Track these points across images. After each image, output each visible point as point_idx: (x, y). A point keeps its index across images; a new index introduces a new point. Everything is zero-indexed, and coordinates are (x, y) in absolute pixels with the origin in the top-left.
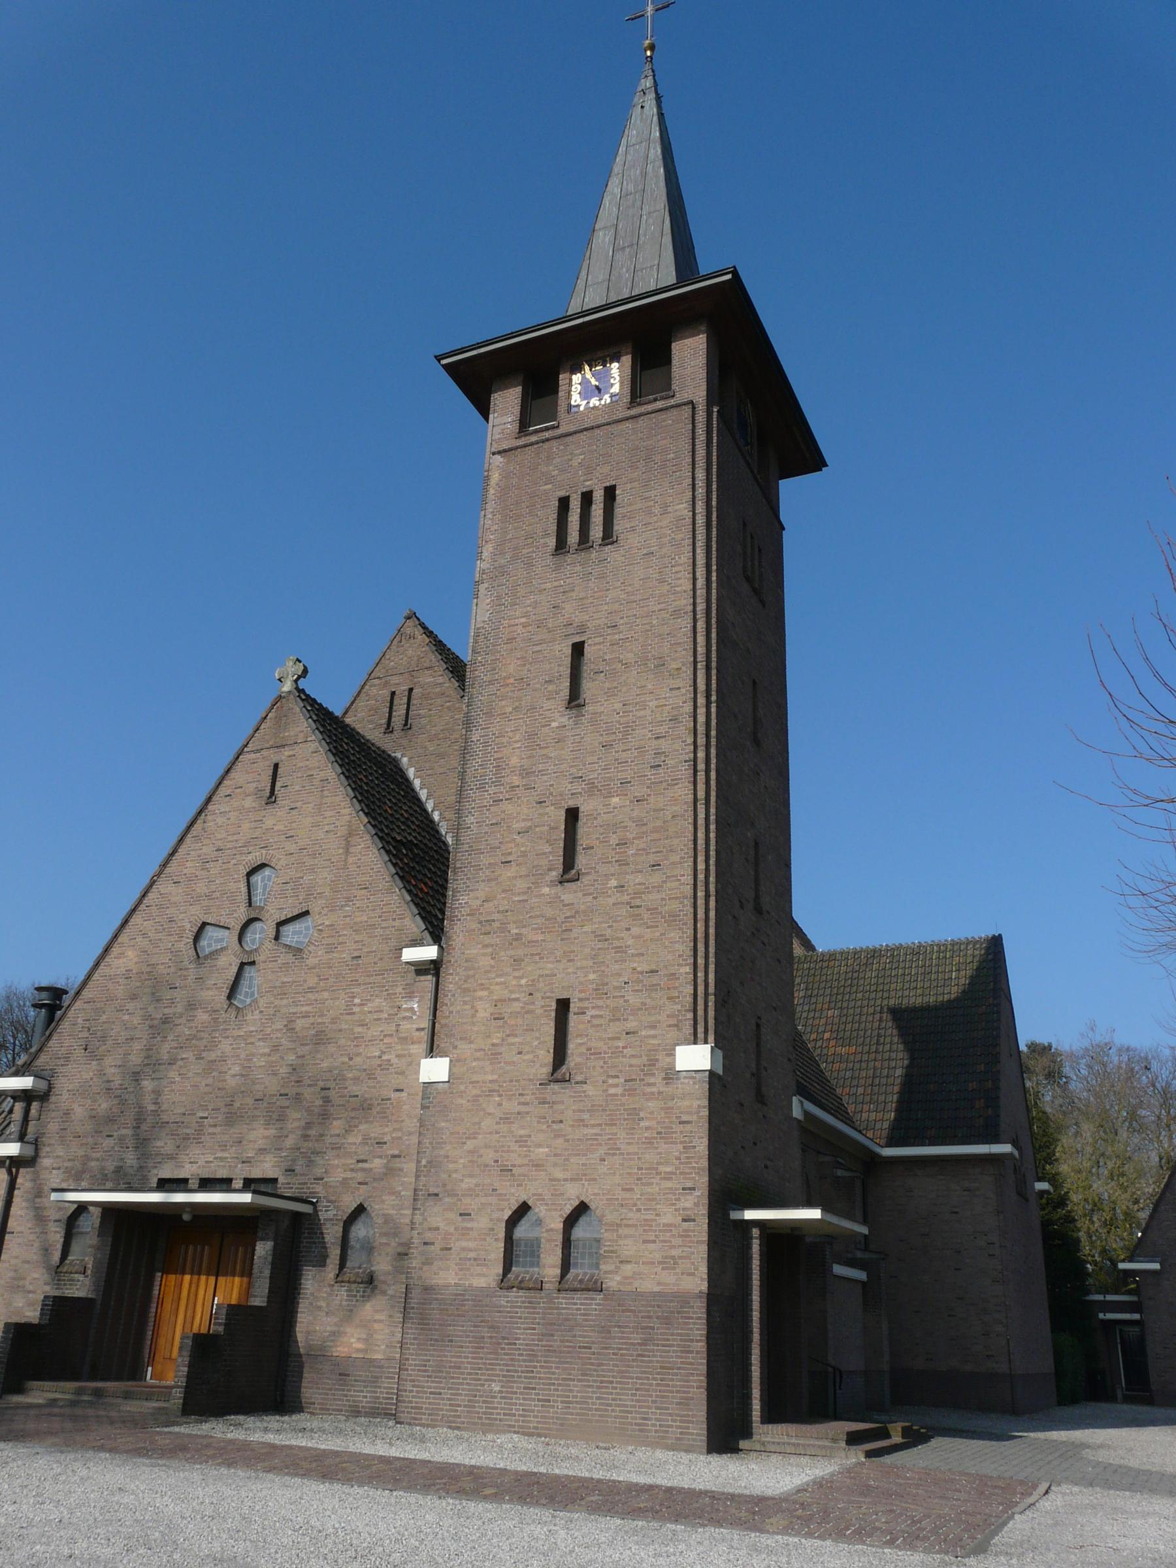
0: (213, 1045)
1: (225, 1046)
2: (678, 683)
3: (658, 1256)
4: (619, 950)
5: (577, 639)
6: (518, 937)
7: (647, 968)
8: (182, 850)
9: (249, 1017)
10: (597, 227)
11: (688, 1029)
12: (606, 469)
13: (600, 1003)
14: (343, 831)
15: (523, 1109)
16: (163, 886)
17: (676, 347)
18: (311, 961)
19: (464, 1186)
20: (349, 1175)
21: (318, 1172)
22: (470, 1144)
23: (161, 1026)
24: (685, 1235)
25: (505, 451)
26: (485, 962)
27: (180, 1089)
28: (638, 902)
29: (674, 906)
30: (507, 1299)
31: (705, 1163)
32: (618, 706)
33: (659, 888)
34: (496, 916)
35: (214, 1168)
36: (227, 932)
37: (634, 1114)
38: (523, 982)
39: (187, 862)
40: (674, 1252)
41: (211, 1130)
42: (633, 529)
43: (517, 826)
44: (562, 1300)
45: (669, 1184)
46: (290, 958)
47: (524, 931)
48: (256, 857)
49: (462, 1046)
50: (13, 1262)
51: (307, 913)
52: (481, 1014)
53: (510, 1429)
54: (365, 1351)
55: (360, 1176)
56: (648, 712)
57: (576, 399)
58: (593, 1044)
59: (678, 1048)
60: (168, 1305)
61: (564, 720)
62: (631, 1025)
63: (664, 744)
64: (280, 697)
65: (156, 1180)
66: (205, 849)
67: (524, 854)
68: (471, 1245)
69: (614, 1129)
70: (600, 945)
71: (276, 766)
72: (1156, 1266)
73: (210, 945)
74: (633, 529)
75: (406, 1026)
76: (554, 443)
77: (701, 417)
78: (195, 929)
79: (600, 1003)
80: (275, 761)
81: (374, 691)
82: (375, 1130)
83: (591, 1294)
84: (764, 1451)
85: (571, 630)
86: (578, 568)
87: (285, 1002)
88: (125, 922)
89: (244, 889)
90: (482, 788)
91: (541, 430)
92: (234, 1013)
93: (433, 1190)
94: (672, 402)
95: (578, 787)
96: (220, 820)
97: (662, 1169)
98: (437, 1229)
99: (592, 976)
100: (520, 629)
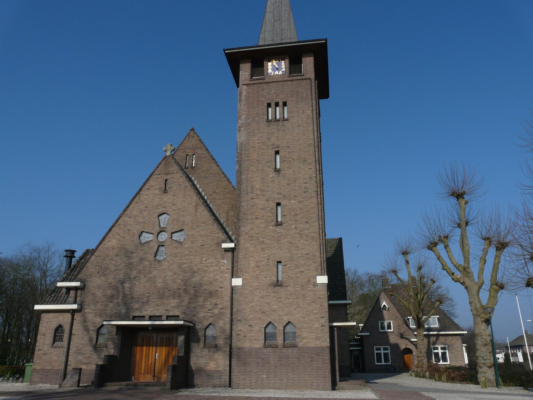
0: (150, 272)
1: (155, 273)
2: (310, 167)
3: (314, 337)
4: (296, 247)
5: (277, 150)
6: (263, 242)
7: (306, 253)
8: (131, 206)
9: (163, 263)
10: (267, 11)
11: (319, 271)
12: (283, 96)
13: (291, 263)
14: (194, 204)
15: (268, 294)
16: (124, 218)
17: (304, 60)
18: (186, 246)
19: (249, 317)
20: (206, 314)
21: (195, 313)
22: (251, 305)
23: (130, 266)
24: (322, 330)
25: (247, 84)
26: (252, 249)
27: (140, 287)
28: (302, 233)
29: (313, 235)
30: (265, 351)
31: (327, 310)
32: (292, 172)
33: (308, 229)
34: (255, 235)
35: (163, 311)
36: (151, 235)
37: (304, 296)
38: (265, 255)
39: (134, 209)
40: (319, 335)
41: (152, 300)
42: (293, 117)
43: (260, 207)
44: (284, 350)
45: (316, 316)
46: (177, 244)
47: (264, 240)
48: (162, 210)
49: (246, 275)
50: (76, 344)
51: (183, 230)
52: (252, 265)
53: (270, 388)
54: (216, 368)
55: (209, 315)
56: (302, 175)
57: (270, 71)
58: (290, 275)
59: (317, 277)
60: (138, 356)
61: (274, 175)
62: (302, 269)
63: (307, 185)
64: (166, 157)
65: (132, 316)
66: (140, 207)
67: (263, 216)
68: (253, 335)
69: (298, 300)
70: (290, 245)
71: (166, 180)
72: (368, 334)
73: (144, 239)
74: (293, 117)
75: (222, 268)
76: (265, 85)
77: (313, 83)
78: (139, 233)
79: (291, 263)
80: (166, 178)
81: (180, 154)
82: (214, 301)
83: (293, 348)
84: (343, 389)
85: (274, 146)
86: (275, 127)
87: (177, 259)
88: (110, 230)
89: (157, 221)
90: (247, 194)
91: (257, 79)
92: (157, 263)
93: (239, 319)
94: (303, 77)
95: (280, 196)
96: (146, 197)
97: (314, 312)
98: (241, 330)
99: (288, 255)
100: (256, 144)
